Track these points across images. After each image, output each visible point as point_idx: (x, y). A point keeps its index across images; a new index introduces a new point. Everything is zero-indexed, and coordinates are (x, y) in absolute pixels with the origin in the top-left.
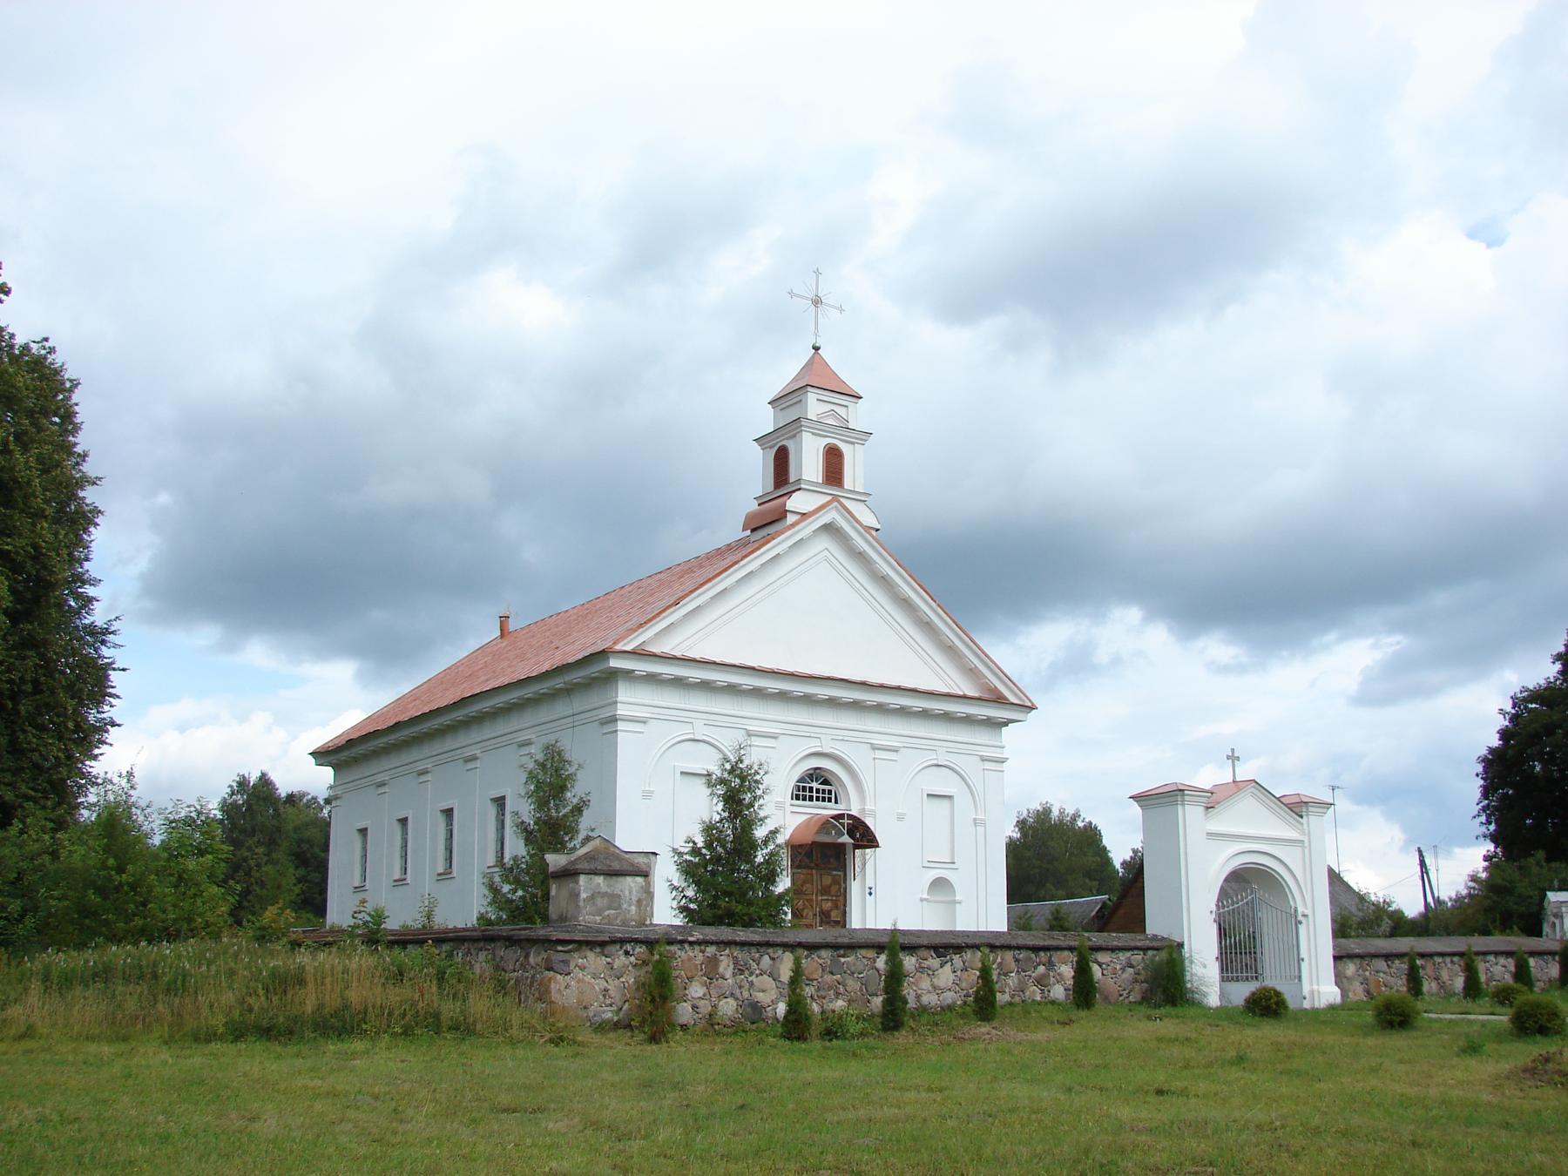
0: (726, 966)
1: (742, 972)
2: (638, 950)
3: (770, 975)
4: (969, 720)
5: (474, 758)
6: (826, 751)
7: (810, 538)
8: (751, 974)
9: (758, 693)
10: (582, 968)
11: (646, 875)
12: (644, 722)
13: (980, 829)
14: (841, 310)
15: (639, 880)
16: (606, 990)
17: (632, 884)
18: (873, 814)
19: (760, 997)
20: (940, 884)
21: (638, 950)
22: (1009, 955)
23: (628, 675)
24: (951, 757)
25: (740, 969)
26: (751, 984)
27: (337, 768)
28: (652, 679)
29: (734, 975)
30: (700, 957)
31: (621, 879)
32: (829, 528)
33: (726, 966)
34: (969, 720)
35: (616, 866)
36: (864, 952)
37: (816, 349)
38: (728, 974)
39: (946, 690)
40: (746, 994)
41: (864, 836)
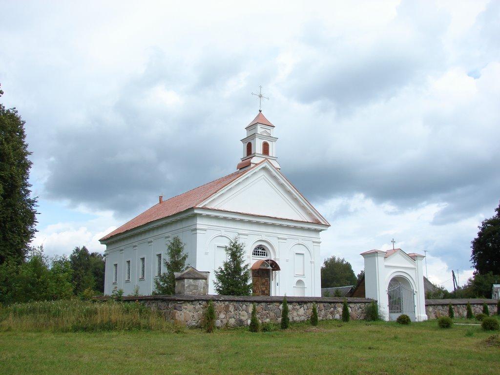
0: (231, 308)
1: (236, 310)
2: (203, 303)
10: (186, 309)
11: (206, 279)
15: (204, 280)
16: (193, 316)
17: (202, 282)
19: (242, 318)
21: (203, 303)
22: (322, 305)
23: (200, 215)
25: (236, 309)
26: (240, 314)
28: (208, 216)
29: (234, 311)
32: (264, 169)
33: (231, 308)
34: (309, 230)
35: (197, 276)
36: (275, 303)
37: (260, 111)
38: (232, 311)
41: (275, 267)
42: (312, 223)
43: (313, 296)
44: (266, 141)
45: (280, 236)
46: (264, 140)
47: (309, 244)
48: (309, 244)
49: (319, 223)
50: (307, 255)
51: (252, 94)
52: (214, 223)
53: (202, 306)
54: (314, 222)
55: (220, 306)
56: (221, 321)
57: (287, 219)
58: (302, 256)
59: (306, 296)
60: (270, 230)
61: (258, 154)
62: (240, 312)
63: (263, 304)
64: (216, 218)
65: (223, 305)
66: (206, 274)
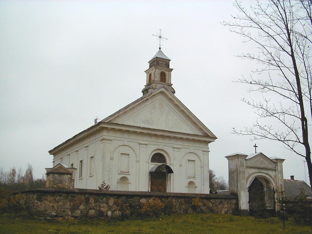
0: (92, 200)
1: (97, 202)
2: (64, 195)
3: (106, 203)
4: (199, 141)
5: (78, 151)
6: (160, 148)
7: (158, 93)
8: (100, 203)
9: (142, 134)
10: (46, 200)
11: (71, 174)
12: (111, 140)
13: (202, 169)
14: (153, 35)
15: (69, 176)
16: (53, 206)
17: (66, 177)
18: (173, 165)
19: (102, 209)
20: (191, 183)
21: (64, 195)
22: (183, 200)
23: (106, 128)
24: (195, 151)
25: (96, 201)
26: (100, 206)
27: (54, 154)
28: (113, 130)
29: (94, 203)
30: (84, 197)
31: (63, 176)
32: (162, 92)
33: (92, 200)
34: (199, 141)
35: (62, 171)
36: (136, 197)
37: (160, 48)
38: (92, 202)
39: (193, 134)
40: (98, 208)
41: (170, 171)
42: (203, 136)
43: (137, 190)
44: (163, 71)
45: (140, 142)
46: (162, 71)
47: (200, 153)
48: (200, 153)
49: (208, 136)
50: (198, 162)
51: (153, 35)
52: (118, 135)
53: (62, 197)
54: (204, 135)
55: (80, 198)
56: (81, 212)
57: (179, 133)
58: (126, 157)
59: (129, 190)
60: (167, 141)
61: (157, 81)
62: (101, 204)
63: (123, 198)
64: (120, 131)
65: (84, 197)
66: (71, 170)
